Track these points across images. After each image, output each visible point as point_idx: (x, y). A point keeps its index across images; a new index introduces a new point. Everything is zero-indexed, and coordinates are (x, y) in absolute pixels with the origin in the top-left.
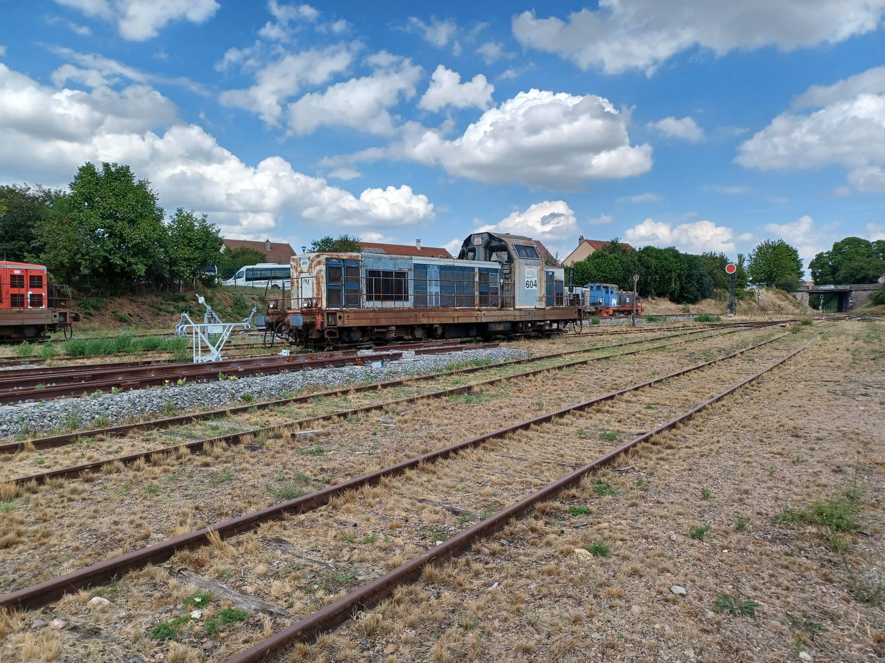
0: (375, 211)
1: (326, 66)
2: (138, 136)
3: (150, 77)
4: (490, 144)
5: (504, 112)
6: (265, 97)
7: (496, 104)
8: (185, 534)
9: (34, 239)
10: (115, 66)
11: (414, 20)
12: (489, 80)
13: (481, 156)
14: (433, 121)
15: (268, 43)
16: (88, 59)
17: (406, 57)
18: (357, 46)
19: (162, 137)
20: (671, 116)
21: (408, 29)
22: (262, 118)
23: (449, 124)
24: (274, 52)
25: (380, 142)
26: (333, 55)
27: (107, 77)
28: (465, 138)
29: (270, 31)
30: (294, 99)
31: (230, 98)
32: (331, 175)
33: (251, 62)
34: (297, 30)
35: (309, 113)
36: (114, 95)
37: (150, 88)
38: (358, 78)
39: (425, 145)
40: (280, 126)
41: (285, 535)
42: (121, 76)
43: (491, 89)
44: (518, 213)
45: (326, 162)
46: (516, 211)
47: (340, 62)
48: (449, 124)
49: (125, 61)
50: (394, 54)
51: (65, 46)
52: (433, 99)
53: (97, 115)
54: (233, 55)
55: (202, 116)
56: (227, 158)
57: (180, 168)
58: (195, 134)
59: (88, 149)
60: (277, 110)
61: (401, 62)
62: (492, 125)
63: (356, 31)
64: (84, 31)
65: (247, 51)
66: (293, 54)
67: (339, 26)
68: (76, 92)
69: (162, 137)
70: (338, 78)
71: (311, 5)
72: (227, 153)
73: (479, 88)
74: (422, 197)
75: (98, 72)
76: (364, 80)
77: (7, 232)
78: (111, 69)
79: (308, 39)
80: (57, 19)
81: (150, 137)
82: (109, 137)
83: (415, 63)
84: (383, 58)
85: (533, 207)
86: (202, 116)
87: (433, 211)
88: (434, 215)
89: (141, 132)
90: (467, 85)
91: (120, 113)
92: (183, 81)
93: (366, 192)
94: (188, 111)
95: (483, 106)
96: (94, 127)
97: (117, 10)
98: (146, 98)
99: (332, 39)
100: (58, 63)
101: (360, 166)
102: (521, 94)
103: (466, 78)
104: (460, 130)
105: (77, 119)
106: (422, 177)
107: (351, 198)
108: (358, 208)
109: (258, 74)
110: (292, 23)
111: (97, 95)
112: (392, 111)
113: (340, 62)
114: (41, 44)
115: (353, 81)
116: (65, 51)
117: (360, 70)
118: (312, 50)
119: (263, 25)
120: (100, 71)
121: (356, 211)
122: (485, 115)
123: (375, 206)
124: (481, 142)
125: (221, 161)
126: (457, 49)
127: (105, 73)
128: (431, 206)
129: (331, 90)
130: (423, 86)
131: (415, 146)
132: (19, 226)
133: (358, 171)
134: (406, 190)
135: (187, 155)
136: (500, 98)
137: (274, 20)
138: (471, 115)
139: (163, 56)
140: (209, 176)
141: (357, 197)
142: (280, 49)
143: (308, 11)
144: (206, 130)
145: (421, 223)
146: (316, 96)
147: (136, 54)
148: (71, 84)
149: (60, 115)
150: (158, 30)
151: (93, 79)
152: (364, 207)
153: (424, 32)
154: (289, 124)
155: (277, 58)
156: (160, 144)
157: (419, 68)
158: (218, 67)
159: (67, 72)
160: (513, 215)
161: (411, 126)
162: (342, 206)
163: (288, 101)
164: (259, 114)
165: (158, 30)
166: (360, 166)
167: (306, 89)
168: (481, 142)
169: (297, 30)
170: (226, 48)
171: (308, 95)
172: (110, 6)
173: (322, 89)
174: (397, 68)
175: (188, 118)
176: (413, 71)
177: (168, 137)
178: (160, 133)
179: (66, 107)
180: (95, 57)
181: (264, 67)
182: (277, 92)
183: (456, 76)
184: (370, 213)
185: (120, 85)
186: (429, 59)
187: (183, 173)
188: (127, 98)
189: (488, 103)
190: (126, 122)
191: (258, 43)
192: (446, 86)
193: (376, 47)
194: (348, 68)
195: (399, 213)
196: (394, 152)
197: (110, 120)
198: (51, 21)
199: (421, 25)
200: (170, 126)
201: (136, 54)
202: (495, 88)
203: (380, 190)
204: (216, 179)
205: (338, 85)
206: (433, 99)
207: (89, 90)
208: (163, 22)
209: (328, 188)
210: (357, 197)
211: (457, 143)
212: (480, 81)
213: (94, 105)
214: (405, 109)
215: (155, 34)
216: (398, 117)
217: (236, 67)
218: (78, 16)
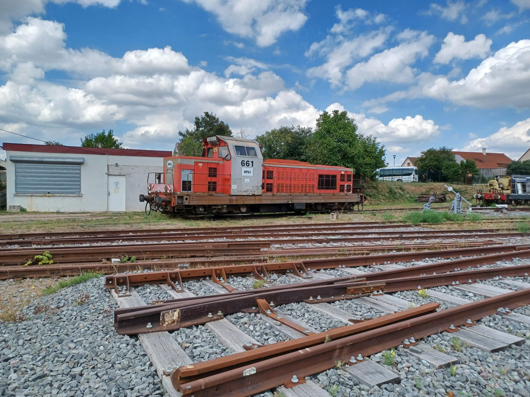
0: (397, 133)
1: (368, 45)
2: (262, 100)
3: (270, 66)
4: (487, 81)
5: (498, 58)
6: (332, 69)
7: (492, 53)
8: (417, 308)
9: (302, 155)
10: (253, 62)
11: (434, 6)
12: (488, 36)
13: (480, 90)
14: (444, 70)
15: (334, 35)
16: (240, 60)
17: (423, 30)
18: (390, 29)
19: (274, 99)
20: (314, 42)
21: (429, 13)
22: (330, 81)
23: (457, 71)
24: (338, 40)
25: (404, 87)
26: (373, 38)
27: (249, 69)
28: (467, 78)
29: (337, 28)
30: (349, 67)
31: (313, 72)
32: (369, 112)
33: (324, 49)
34: (353, 25)
35: (358, 75)
36: (254, 78)
37: (272, 72)
38: (389, 49)
39: (437, 87)
40: (340, 85)
41: (244, 350)
42: (255, 67)
43: (490, 42)
44: (505, 128)
45: (366, 104)
46: (503, 127)
47: (379, 41)
48: (457, 71)
49: (258, 59)
50: (415, 30)
51: (230, 56)
52: (444, 56)
53: (244, 90)
54: (315, 46)
55: (297, 84)
56: (308, 107)
57: (283, 115)
58: (292, 96)
59: (239, 109)
60: (339, 75)
61: (419, 35)
62: (491, 68)
63: (389, 20)
64: (241, 45)
65: (322, 43)
66: (349, 40)
67: (379, 18)
68: (235, 79)
69: (274, 99)
70: (377, 51)
71: (363, 8)
72: (307, 104)
73: (481, 43)
74: (430, 121)
75: (244, 67)
76: (392, 50)
77: (289, 152)
78: (251, 64)
79: (360, 29)
80: (230, 42)
81: (269, 99)
82: (248, 101)
83: (429, 34)
84: (407, 34)
85: (519, 123)
86: (297, 84)
87: (438, 130)
88: (438, 132)
89: (265, 97)
90: (471, 43)
91: (255, 87)
92: (287, 66)
93: (392, 121)
94: (288, 81)
95: (482, 56)
96: (243, 97)
97: (256, 31)
98: (268, 78)
99: (376, 27)
100: (227, 65)
101: (389, 104)
102: (513, 44)
103: (469, 38)
104: (465, 73)
105: (236, 94)
106: (431, 108)
107: (382, 125)
108: (386, 131)
109: (328, 56)
110: (350, 22)
111: (246, 79)
112: (412, 66)
113: (379, 41)
114: (220, 56)
115: (386, 51)
116: (230, 58)
117: (391, 43)
118: (361, 36)
119: (331, 26)
120: (246, 66)
121: (385, 133)
122: (484, 62)
123: (398, 130)
124: (480, 80)
125: (304, 109)
126: (464, 20)
127: (248, 67)
128: (437, 127)
129: (372, 59)
130: (436, 48)
131: (430, 88)
132: (296, 148)
133: (386, 107)
134: (418, 118)
135: (287, 107)
136: (495, 47)
137: (338, 21)
138: (474, 63)
139: (277, 52)
140: (298, 118)
141: (386, 124)
142: (341, 38)
143: (360, 13)
144: (297, 92)
145: (431, 137)
146: (362, 63)
147: (265, 55)
148: (233, 76)
149: (229, 93)
150: (276, 39)
151: (243, 71)
152: (390, 131)
153: (441, 13)
154: (346, 83)
155: (339, 44)
156: (273, 102)
157: (432, 37)
158: (307, 54)
159: (232, 69)
160: (502, 130)
161: (425, 76)
162: (377, 131)
163: (345, 69)
164: (329, 79)
165: (276, 39)
166: (389, 104)
167: (357, 60)
168: (480, 80)
169: (353, 25)
170: (310, 44)
171: (358, 64)
172: (253, 30)
173: (366, 59)
174: (417, 38)
175: (289, 85)
176: (427, 39)
177: (278, 98)
178: (274, 96)
179: (232, 87)
180: (244, 59)
181: (332, 51)
182: (337, 65)
183: (462, 38)
184: (394, 134)
185: (256, 72)
186: (440, 30)
187: (285, 118)
188: (260, 79)
189: (486, 53)
190: (258, 92)
191: (328, 37)
192: (454, 46)
193: (402, 27)
194: (384, 44)
195: (413, 132)
196: (413, 93)
197: (250, 92)
198: (226, 43)
199: (439, 8)
200: (279, 91)
201: (265, 55)
202: (493, 41)
203: (401, 120)
204: (302, 120)
205: (376, 55)
206: (444, 56)
207: (241, 77)
208: (278, 34)
209: (366, 119)
210: (386, 124)
211: (461, 82)
212: (480, 39)
213: (244, 85)
214: (423, 65)
215: (275, 41)
216: (415, 69)
217: (316, 53)
218: (238, 39)
